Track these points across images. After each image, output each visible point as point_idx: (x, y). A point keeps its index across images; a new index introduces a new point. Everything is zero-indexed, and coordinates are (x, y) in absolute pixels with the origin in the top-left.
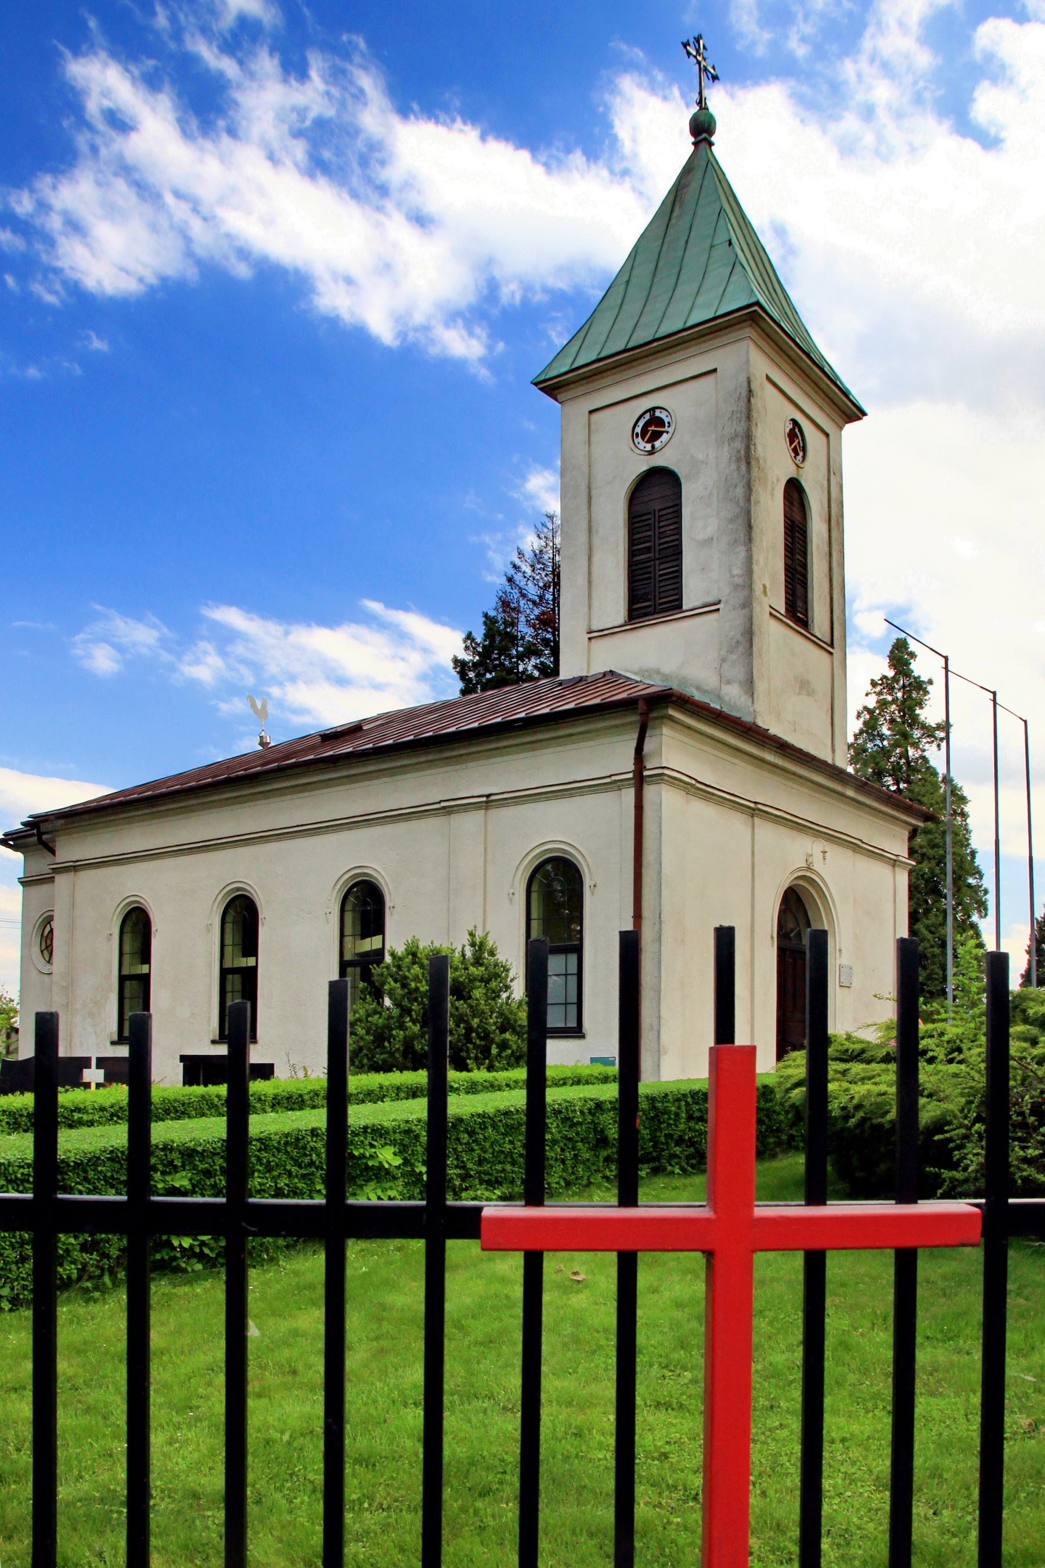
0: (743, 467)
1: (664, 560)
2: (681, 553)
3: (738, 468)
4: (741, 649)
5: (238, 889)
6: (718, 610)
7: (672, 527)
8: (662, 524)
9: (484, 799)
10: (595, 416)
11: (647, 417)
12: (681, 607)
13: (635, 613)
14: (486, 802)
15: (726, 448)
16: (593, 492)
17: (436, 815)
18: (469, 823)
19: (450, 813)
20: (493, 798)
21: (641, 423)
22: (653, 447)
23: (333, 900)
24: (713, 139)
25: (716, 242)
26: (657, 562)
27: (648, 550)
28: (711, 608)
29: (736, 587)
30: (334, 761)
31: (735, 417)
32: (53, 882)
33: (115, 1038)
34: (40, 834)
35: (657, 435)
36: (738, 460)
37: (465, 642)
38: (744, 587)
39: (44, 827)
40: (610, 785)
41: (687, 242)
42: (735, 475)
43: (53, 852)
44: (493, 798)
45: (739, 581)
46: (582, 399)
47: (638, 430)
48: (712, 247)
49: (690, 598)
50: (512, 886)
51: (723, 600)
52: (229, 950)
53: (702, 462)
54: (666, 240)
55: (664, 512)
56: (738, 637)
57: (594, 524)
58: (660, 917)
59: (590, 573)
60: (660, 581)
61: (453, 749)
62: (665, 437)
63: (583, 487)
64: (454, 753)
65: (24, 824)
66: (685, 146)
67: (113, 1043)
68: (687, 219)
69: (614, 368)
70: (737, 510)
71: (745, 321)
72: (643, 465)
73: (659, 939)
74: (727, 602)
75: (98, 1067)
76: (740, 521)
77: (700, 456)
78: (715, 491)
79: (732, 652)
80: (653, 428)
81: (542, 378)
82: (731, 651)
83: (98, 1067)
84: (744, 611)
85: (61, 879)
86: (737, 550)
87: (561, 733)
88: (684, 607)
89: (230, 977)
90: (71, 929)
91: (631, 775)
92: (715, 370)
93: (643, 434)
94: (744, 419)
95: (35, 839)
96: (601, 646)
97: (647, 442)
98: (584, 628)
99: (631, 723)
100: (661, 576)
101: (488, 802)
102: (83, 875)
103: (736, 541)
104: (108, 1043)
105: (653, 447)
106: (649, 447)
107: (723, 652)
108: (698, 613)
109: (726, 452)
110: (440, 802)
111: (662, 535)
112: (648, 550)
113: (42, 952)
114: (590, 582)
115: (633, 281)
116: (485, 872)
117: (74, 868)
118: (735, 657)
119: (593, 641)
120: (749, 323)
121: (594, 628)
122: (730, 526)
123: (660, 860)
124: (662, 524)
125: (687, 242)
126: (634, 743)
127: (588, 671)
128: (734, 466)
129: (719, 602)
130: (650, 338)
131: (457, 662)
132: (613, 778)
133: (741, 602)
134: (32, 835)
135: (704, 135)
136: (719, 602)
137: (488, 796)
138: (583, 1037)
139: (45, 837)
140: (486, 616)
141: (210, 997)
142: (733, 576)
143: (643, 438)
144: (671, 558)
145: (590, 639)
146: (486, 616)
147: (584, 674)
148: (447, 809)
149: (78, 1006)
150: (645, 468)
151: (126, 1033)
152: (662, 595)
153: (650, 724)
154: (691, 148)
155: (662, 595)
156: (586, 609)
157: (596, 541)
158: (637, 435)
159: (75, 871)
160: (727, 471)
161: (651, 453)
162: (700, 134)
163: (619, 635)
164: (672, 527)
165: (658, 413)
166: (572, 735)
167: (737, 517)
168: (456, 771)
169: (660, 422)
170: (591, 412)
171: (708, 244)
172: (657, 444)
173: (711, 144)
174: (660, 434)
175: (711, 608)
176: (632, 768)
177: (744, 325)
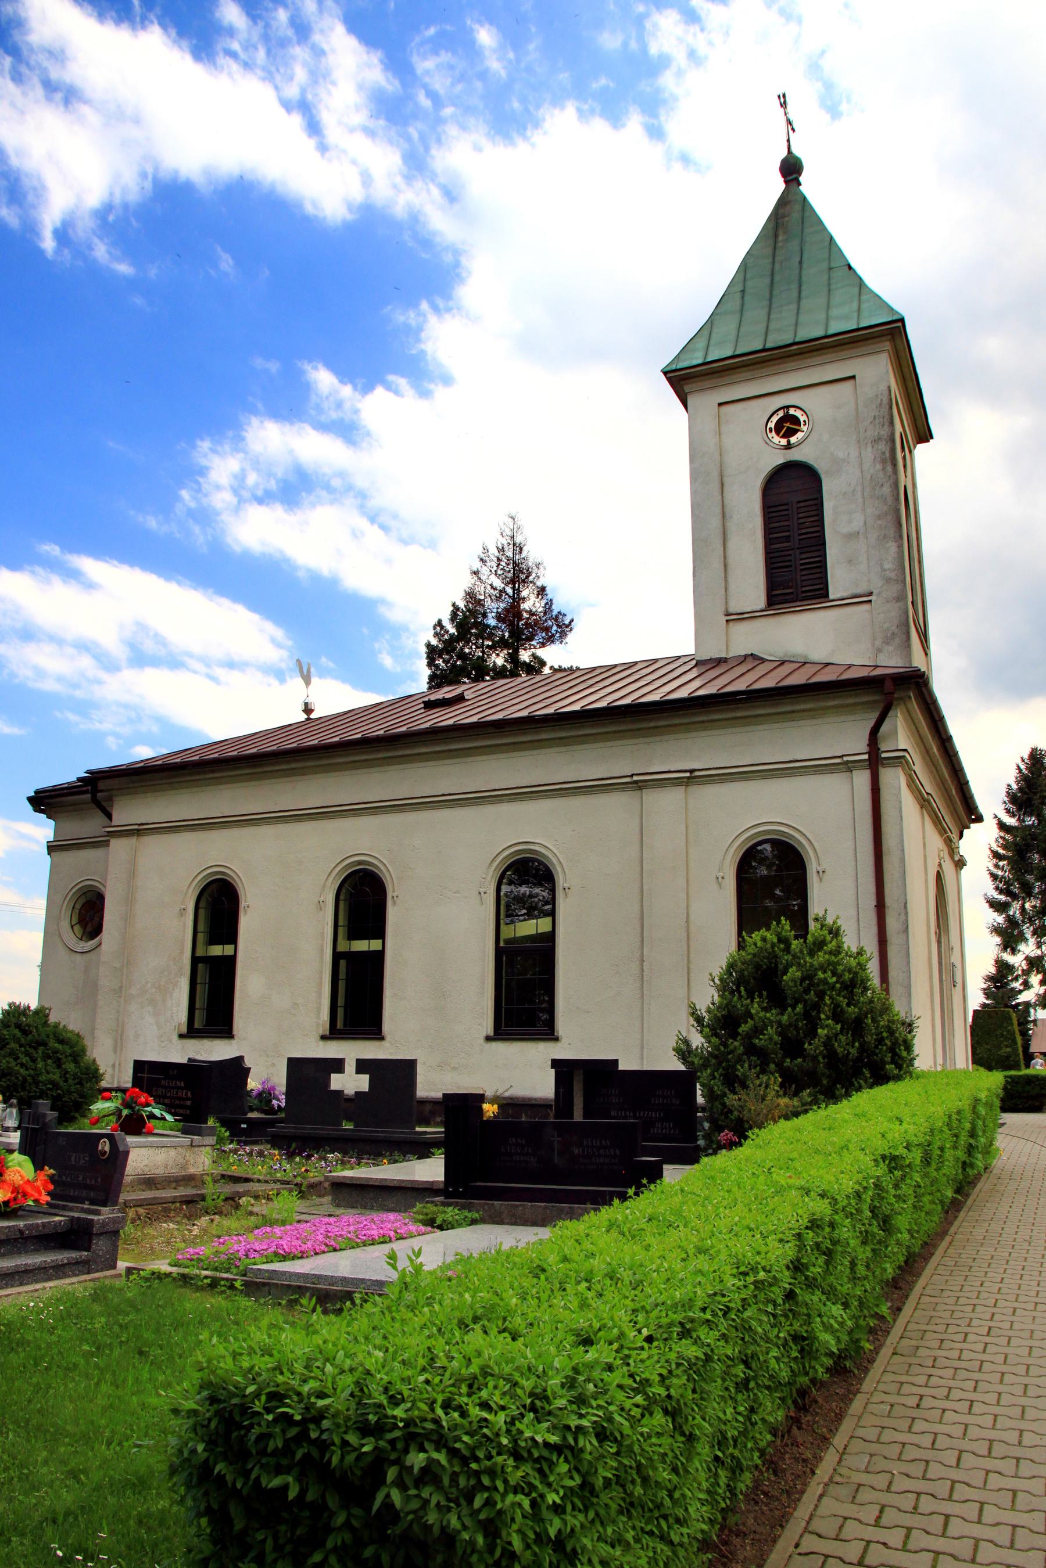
0: (889, 468)
1: (805, 550)
2: (824, 544)
3: (884, 469)
4: (897, 641)
5: (360, 863)
6: (870, 601)
7: (812, 519)
8: (801, 515)
9: (688, 774)
10: (724, 408)
11: (781, 414)
12: (827, 596)
13: (774, 599)
14: (688, 778)
15: (869, 449)
16: (725, 480)
17: (623, 790)
18: (670, 799)
19: (640, 788)
20: (697, 774)
21: (775, 419)
22: (789, 442)
23: (489, 877)
24: (801, 179)
25: (833, 265)
26: (798, 551)
27: (787, 539)
28: (863, 599)
29: (888, 580)
30: (435, 734)
31: (877, 421)
32: (108, 845)
33: (184, 1029)
34: (95, 792)
35: (792, 432)
36: (883, 461)
37: (435, 628)
38: (897, 581)
39: (101, 785)
40: (846, 766)
41: (801, 262)
42: (881, 475)
43: (109, 816)
44: (697, 774)
45: (893, 575)
46: (709, 392)
47: (772, 425)
48: (830, 269)
49: (835, 590)
50: (720, 869)
51: (875, 592)
52: (201, 937)
53: (843, 460)
54: (777, 259)
55: (802, 504)
56: (894, 628)
57: (727, 510)
58: (905, 907)
59: (725, 557)
60: (802, 570)
61: (651, 720)
62: (800, 435)
63: (715, 474)
64: (652, 724)
65: (79, 779)
66: (779, 185)
67: (323, 1038)
68: (794, 245)
69: (755, 364)
70: (885, 508)
71: (884, 336)
72: (780, 458)
73: (906, 930)
74: (879, 594)
75: (359, 1071)
76: (889, 518)
77: (841, 455)
78: (859, 488)
79: (888, 644)
80: (788, 425)
81: (674, 367)
82: (887, 641)
83: (359, 1071)
84: (898, 604)
85: (114, 843)
86: (887, 545)
87: (739, 714)
88: (831, 597)
89: (200, 966)
90: (130, 900)
91: (866, 757)
92: (853, 377)
93: (778, 428)
94: (887, 424)
95: (89, 796)
96: (741, 630)
97: (782, 437)
98: (721, 610)
99: (874, 702)
100: (802, 564)
101: (691, 779)
102: (149, 840)
103: (885, 536)
104: (175, 1037)
105: (789, 442)
106: (784, 442)
107: (878, 643)
108: (844, 603)
109: (869, 454)
110: (632, 776)
111: (801, 526)
112: (787, 539)
113: (72, 927)
114: (725, 566)
115: (748, 291)
116: (687, 853)
117: (138, 831)
118: (891, 648)
119: (731, 624)
120: (889, 337)
121: (731, 610)
122: (879, 522)
123: (903, 846)
124: (801, 515)
125: (801, 262)
126: (871, 723)
127: (727, 652)
128: (879, 467)
129: (871, 594)
130: (791, 341)
131: (429, 645)
132: (845, 759)
133: (895, 595)
134: (86, 792)
135: (794, 176)
136: (871, 594)
137: (691, 771)
138: (382, 1039)
139: (99, 795)
140: (454, 605)
141: (320, 985)
142: (885, 570)
143: (778, 433)
144: (814, 548)
145: (727, 621)
146: (454, 605)
147: (723, 655)
148: (638, 785)
149: (134, 991)
150: (781, 461)
151: (340, 1025)
152: (804, 584)
153: (895, 703)
154: (783, 186)
155: (804, 584)
156: (723, 592)
157: (731, 526)
158: (771, 430)
159: (139, 835)
160: (872, 471)
161: (789, 446)
162: (791, 174)
163: (763, 620)
164: (812, 519)
165: (792, 411)
166: (793, 712)
167: (886, 514)
168: (649, 743)
169: (796, 420)
170: (720, 405)
171: (825, 265)
172: (793, 440)
173: (800, 184)
174: (795, 431)
175: (863, 599)
176: (866, 749)
177: (884, 338)
